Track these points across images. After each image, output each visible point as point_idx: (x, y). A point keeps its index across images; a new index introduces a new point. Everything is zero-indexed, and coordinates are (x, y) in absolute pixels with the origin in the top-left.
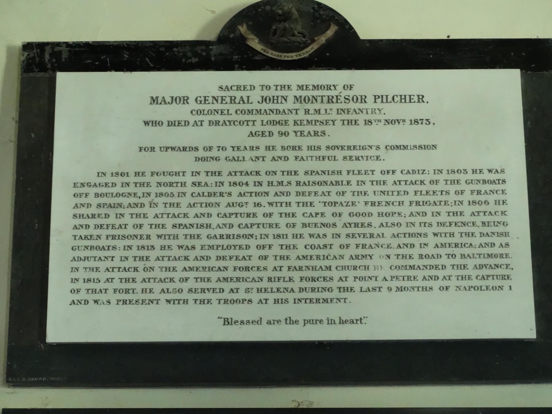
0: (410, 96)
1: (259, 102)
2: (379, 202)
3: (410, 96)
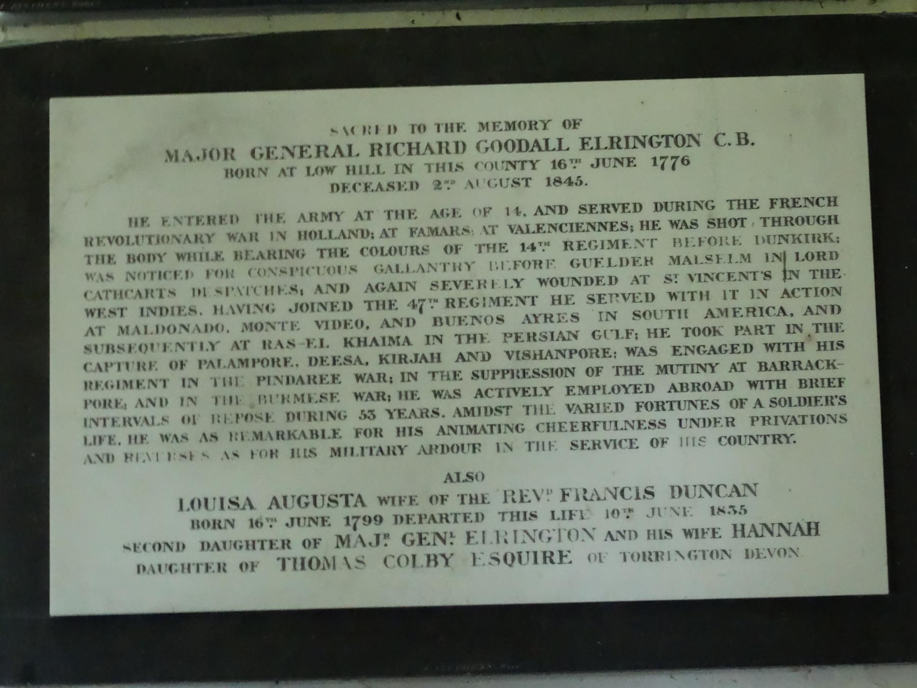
0: (560, 423)
1: (290, 310)
2: (138, 382)
3: (560, 423)
